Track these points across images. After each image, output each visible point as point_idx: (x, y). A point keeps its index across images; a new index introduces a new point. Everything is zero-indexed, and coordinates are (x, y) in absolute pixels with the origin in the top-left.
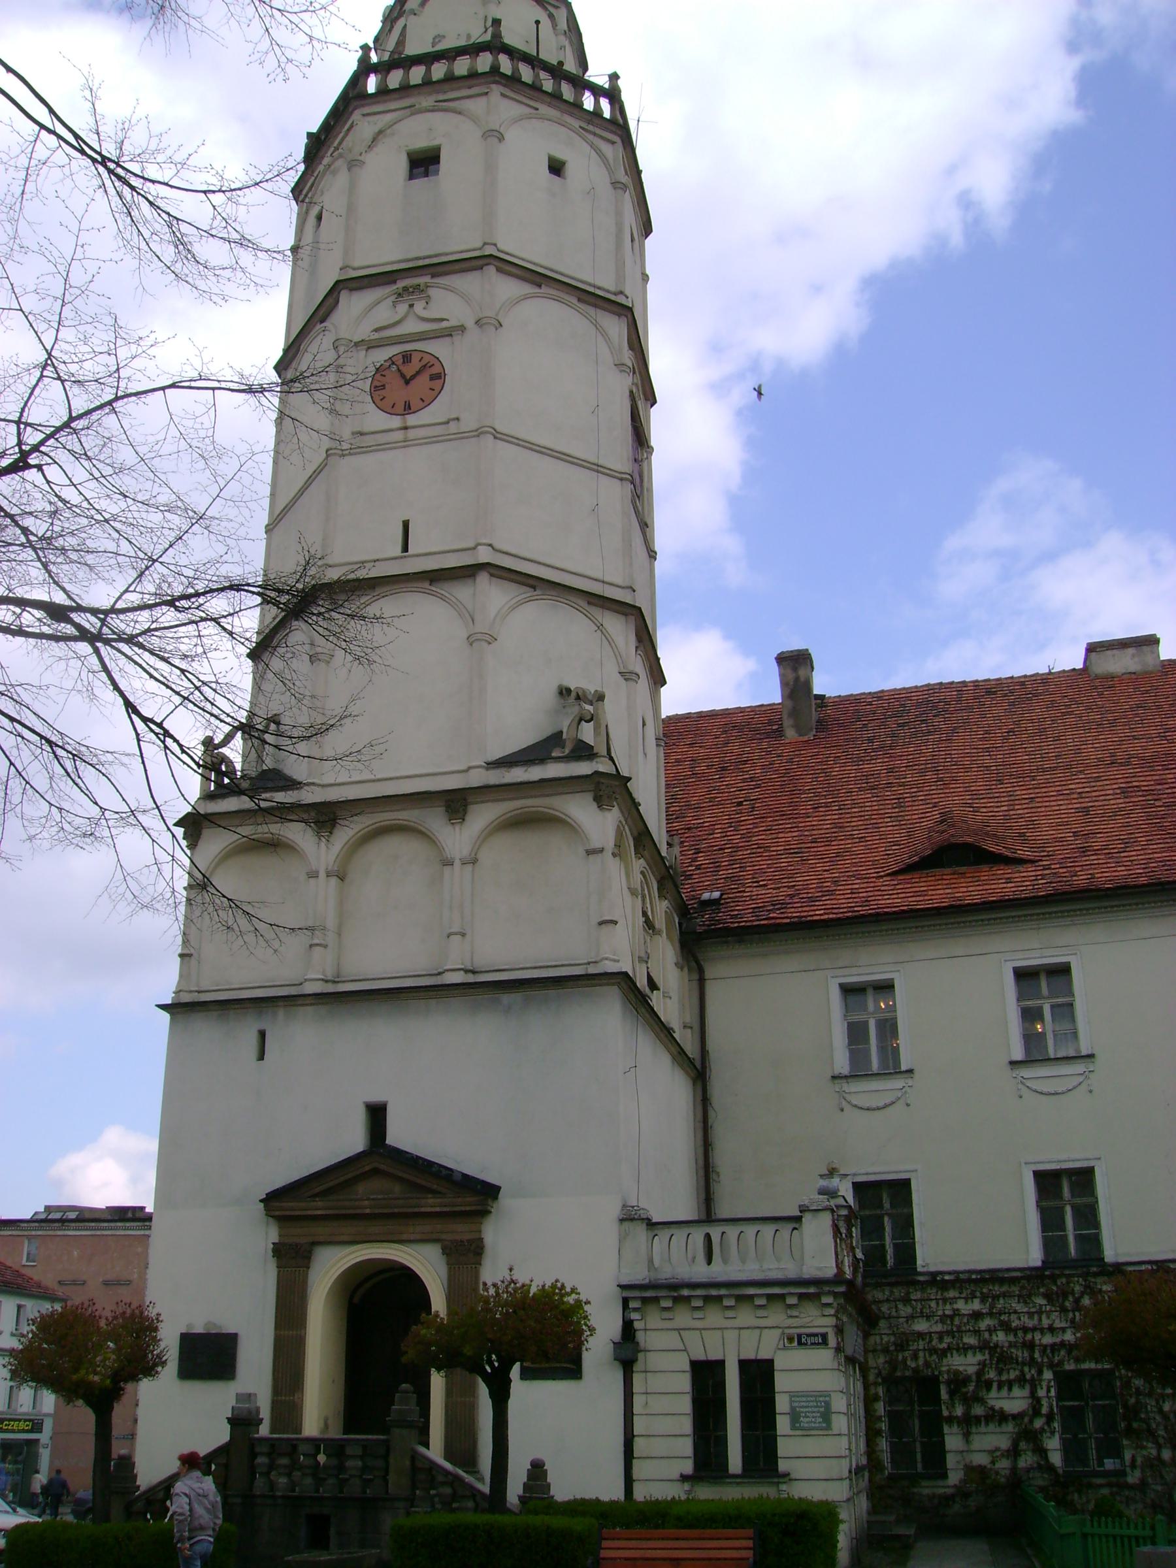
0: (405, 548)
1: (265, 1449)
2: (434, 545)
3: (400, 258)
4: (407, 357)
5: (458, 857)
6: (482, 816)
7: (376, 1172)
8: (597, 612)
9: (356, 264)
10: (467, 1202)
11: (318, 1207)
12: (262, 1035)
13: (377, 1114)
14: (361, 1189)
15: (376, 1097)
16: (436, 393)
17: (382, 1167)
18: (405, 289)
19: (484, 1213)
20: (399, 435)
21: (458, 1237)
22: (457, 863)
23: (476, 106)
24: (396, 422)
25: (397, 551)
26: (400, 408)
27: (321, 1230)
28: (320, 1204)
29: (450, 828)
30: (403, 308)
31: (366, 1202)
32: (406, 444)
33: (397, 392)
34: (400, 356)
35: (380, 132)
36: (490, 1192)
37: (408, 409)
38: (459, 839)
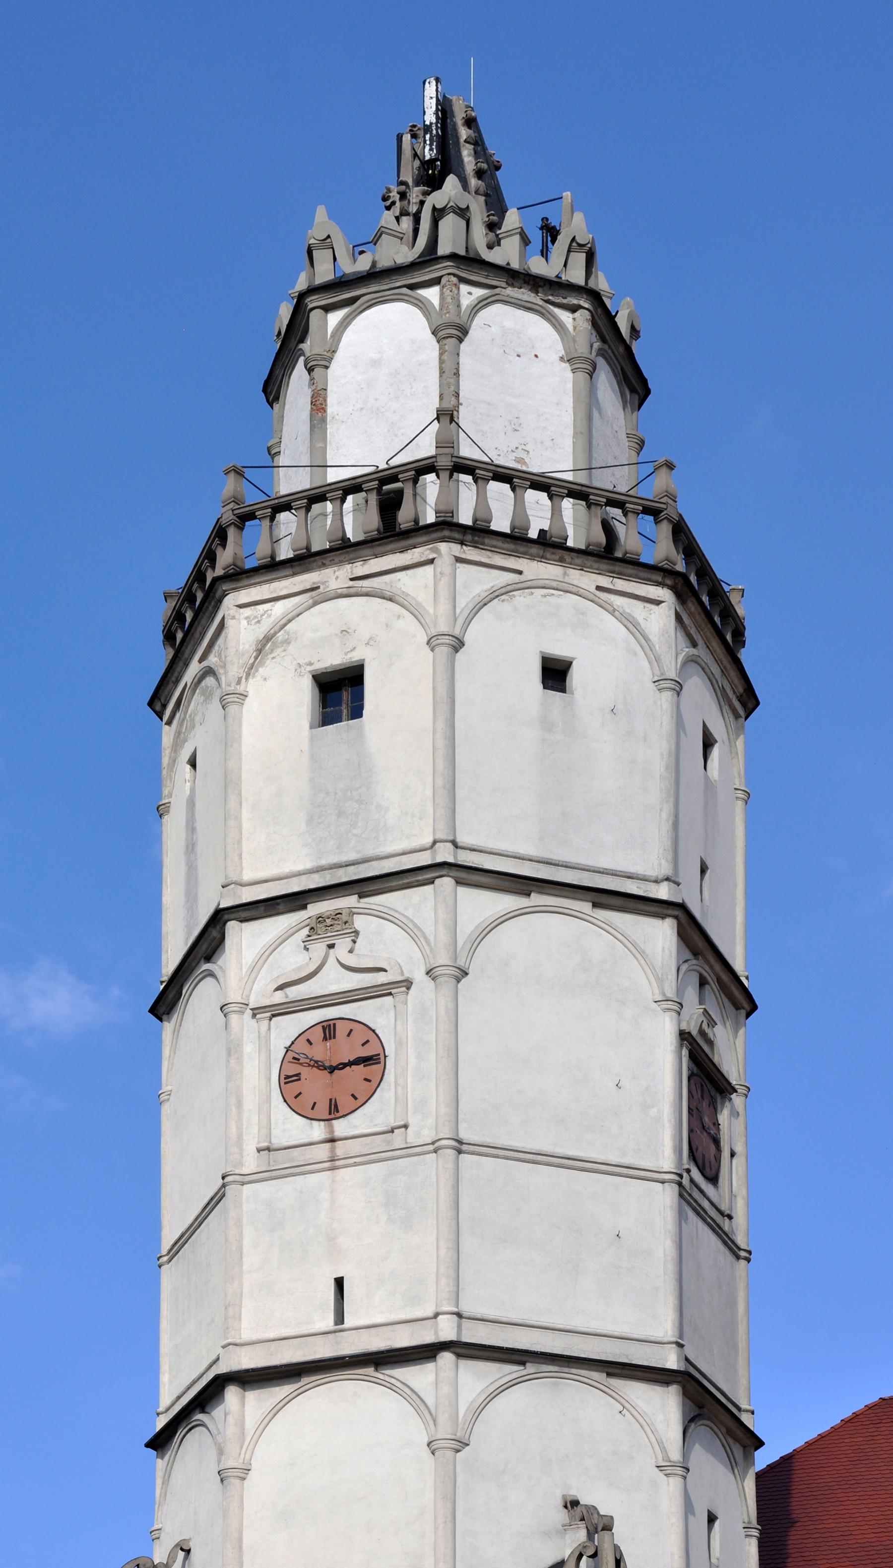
32: (333, 1163)
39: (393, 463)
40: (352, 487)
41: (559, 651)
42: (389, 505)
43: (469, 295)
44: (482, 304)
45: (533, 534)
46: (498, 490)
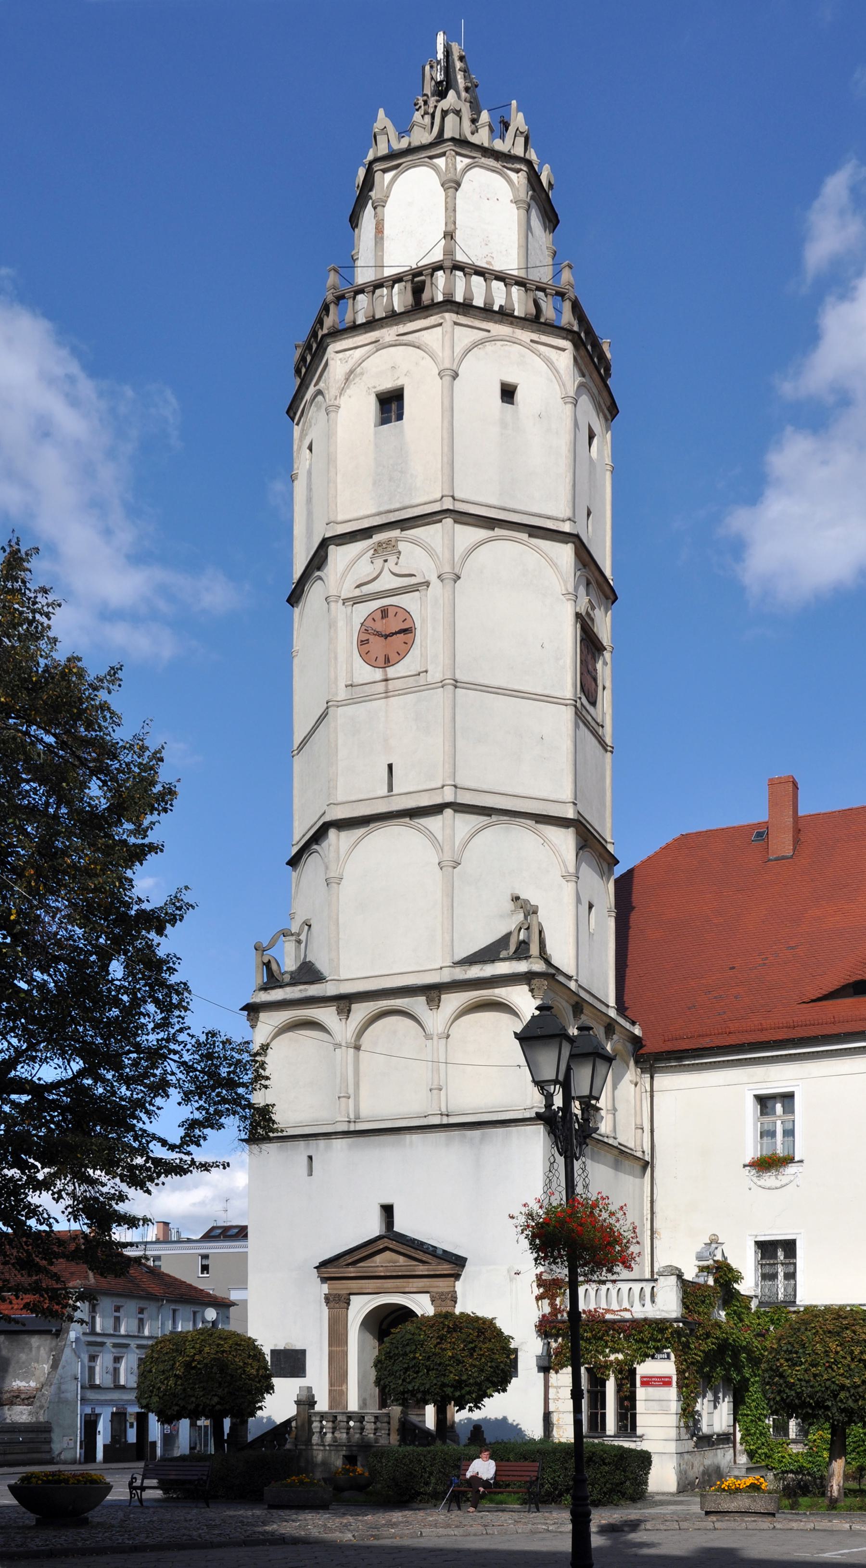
0: (390, 789)
1: (318, 1419)
2: (412, 789)
3: (374, 511)
4: (384, 612)
5: (435, 1034)
6: (452, 1002)
7: (386, 1249)
8: (540, 827)
9: (340, 518)
10: (445, 1268)
11: (351, 1271)
12: (310, 1158)
13: (388, 1210)
14: (378, 1259)
15: (387, 1201)
16: (409, 646)
17: (391, 1246)
18: (380, 544)
19: (457, 1276)
20: (381, 687)
21: (440, 1290)
22: (435, 1038)
23: (432, 338)
24: (378, 674)
25: (384, 791)
26: (381, 659)
27: (354, 1285)
28: (352, 1269)
29: (427, 1007)
30: (379, 562)
31: (381, 1269)
32: (387, 695)
33: (377, 646)
34: (379, 612)
35: (351, 372)
36: (459, 1262)
37: (388, 662)
38: (436, 1019)
39: (420, 264)
40: (397, 279)
41: (510, 379)
42: (418, 290)
43: (461, 162)
44: (468, 168)
45: (496, 308)
46: (498, 287)
